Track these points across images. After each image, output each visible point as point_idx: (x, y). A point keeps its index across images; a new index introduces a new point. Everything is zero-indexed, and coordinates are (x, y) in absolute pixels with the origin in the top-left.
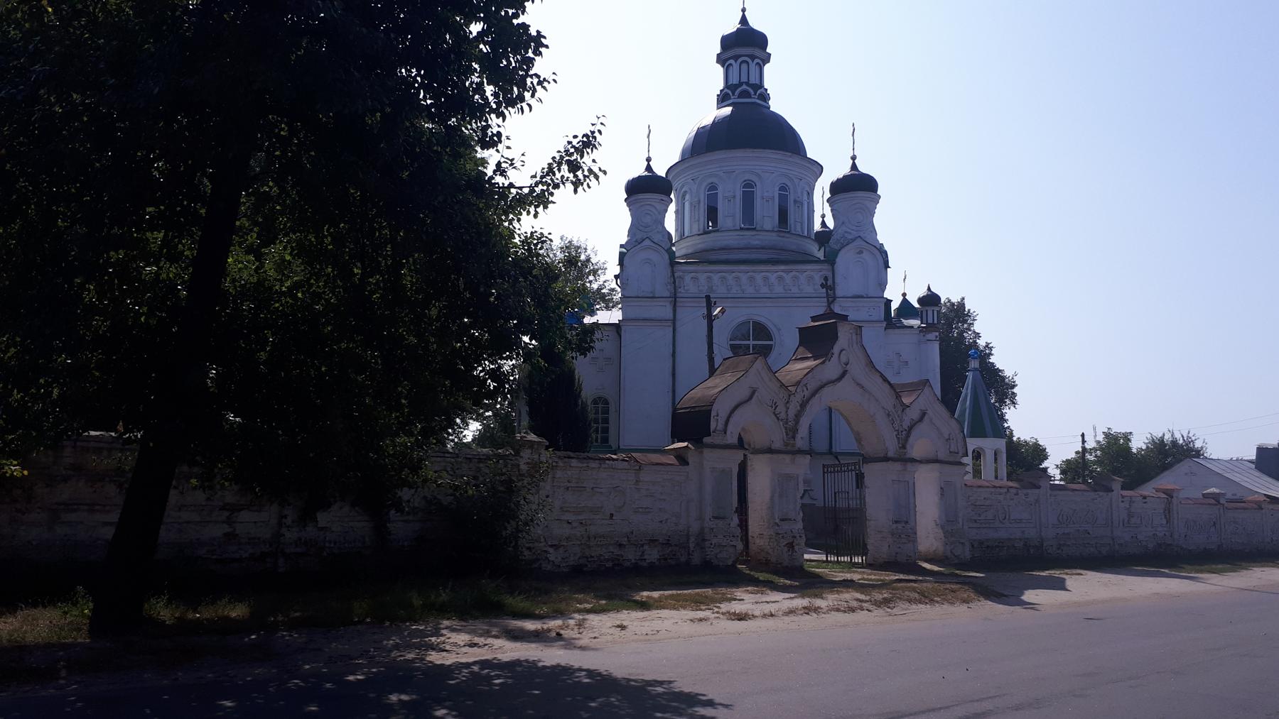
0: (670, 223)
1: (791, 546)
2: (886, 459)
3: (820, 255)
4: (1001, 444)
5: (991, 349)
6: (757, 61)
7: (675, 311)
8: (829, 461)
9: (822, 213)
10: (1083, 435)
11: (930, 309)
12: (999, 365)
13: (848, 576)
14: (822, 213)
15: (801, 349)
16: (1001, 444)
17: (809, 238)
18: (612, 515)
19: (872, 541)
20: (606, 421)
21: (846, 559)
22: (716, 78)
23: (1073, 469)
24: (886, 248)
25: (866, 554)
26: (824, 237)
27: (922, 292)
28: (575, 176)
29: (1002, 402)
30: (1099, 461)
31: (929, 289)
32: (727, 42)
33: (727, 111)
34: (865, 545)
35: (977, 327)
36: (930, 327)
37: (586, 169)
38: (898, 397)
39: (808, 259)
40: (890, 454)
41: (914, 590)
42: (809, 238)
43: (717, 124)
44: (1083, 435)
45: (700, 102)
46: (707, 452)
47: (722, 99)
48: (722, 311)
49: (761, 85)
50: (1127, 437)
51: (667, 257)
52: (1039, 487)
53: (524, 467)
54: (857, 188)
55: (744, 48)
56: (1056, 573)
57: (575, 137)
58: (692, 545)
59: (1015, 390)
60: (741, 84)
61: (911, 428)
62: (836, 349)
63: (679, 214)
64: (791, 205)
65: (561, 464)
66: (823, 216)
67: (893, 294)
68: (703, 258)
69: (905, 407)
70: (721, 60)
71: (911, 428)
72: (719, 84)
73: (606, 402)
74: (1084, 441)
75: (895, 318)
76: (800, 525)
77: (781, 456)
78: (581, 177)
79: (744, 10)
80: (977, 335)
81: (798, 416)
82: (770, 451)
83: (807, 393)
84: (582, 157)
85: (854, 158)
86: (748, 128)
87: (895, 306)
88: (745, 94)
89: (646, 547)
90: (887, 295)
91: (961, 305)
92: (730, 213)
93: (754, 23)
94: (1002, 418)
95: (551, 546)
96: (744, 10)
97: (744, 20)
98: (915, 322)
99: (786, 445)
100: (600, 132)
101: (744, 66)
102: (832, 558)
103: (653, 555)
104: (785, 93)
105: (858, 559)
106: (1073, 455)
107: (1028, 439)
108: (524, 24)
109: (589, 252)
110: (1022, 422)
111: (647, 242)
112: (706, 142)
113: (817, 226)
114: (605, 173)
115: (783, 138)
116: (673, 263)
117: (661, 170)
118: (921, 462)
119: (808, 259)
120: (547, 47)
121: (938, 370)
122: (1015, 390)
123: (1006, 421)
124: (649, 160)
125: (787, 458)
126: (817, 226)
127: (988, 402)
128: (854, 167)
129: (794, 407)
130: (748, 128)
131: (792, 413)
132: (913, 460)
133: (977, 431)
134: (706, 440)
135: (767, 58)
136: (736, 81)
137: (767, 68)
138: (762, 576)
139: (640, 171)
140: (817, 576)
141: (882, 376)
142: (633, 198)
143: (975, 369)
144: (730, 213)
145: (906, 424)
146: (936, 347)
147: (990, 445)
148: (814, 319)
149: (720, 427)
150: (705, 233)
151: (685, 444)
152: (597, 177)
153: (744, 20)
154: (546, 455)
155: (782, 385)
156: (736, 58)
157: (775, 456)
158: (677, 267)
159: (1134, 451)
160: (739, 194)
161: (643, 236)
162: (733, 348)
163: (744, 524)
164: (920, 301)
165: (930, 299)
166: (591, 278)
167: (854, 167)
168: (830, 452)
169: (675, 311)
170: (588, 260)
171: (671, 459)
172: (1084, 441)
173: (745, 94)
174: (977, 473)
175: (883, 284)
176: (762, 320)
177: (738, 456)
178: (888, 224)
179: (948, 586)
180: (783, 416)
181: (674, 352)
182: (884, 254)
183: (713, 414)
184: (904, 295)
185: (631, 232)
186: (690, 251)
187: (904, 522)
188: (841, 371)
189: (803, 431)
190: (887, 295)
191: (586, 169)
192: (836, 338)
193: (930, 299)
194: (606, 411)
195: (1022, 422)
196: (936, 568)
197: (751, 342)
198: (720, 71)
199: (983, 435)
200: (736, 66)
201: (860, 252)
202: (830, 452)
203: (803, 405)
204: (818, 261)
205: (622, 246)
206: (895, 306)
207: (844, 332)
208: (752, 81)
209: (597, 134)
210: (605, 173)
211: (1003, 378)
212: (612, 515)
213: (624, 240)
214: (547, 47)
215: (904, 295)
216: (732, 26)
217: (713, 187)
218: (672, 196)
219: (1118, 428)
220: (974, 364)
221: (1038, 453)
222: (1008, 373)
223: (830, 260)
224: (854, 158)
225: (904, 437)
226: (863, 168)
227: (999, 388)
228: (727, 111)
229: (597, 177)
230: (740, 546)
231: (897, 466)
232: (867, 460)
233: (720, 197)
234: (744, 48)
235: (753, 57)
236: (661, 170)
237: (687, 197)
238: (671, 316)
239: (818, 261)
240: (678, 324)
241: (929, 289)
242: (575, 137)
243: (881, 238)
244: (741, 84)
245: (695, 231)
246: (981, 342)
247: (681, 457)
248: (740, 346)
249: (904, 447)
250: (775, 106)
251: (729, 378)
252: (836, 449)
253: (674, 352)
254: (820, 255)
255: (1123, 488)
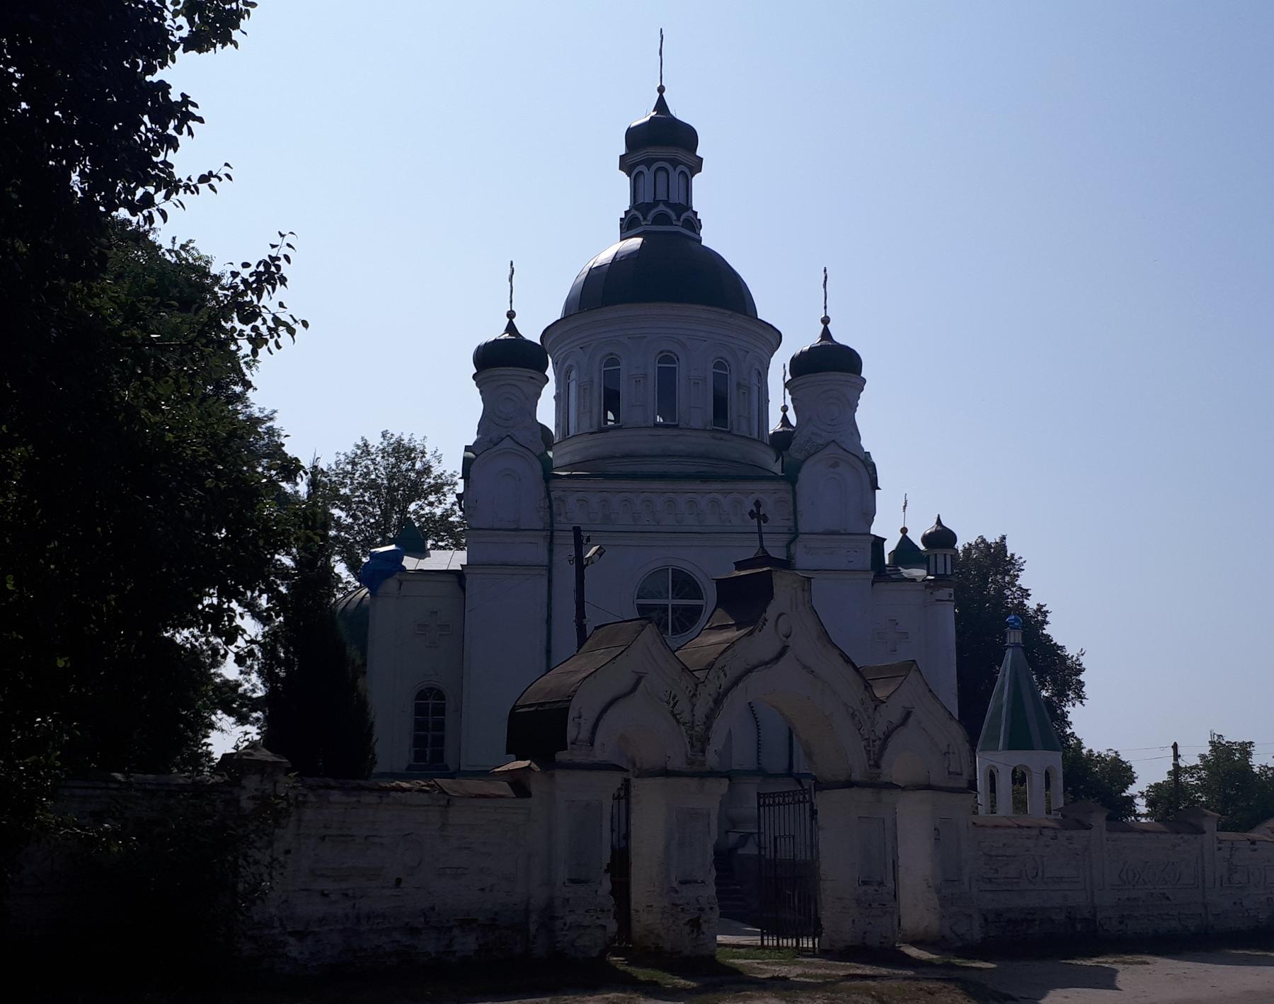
0: (546, 412)
1: (695, 924)
2: (849, 784)
3: (777, 468)
4: (1055, 760)
5: (1045, 614)
6: (681, 168)
7: (551, 551)
8: (788, 785)
9: (779, 405)
10: (1175, 747)
11: (940, 552)
12: (1058, 639)
13: (783, 971)
14: (779, 405)
15: (720, 612)
16: (1055, 760)
17: (760, 441)
18: (399, 881)
19: (827, 916)
20: (440, 726)
21: (791, 942)
22: (617, 193)
23: (1169, 797)
24: (874, 458)
25: (819, 935)
26: (783, 440)
27: (929, 526)
28: (255, 329)
29: (1061, 694)
30: (1203, 788)
31: (939, 522)
32: (635, 137)
33: (635, 243)
34: (818, 920)
35: (1023, 581)
36: (941, 580)
37: (269, 318)
38: (868, 687)
39: (757, 474)
40: (856, 776)
41: (867, 992)
42: (760, 441)
43: (619, 262)
44: (1175, 747)
45: (592, 227)
46: (559, 774)
47: (628, 226)
48: (600, 553)
49: (688, 206)
50: (1246, 749)
51: (538, 466)
52: (1089, 828)
53: (247, 804)
54: (831, 367)
55: (662, 150)
56: (1106, 962)
57: (246, 265)
58: (533, 928)
59: (1082, 677)
60: (656, 203)
61: (888, 736)
62: (772, 611)
63: (561, 399)
64: (734, 392)
65: (312, 798)
66: (785, 409)
67: (887, 527)
68: (597, 470)
69: (878, 703)
70: (626, 164)
71: (888, 736)
72: (622, 202)
73: (440, 695)
74: (1176, 756)
75: (881, 568)
76: (712, 890)
77: (685, 780)
78: (263, 329)
79: (661, 90)
80: (1025, 593)
81: (710, 717)
82: (666, 773)
83: (725, 682)
84: (259, 299)
85: (826, 321)
86: (666, 272)
87: (889, 547)
88: (662, 219)
89: (456, 932)
90: (876, 530)
91: (1001, 546)
92: (638, 395)
93: (678, 110)
94: (1063, 720)
95: (291, 934)
96: (661, 90)
97: (661, 105)
98: (919, 573)
99: (691, 763)
100: (287, 258)
101: (662, 175)
102: (770, 941)
103: (468, 943)
104: (726, 216)
105: (807, 943)
106: (1166, 778)
107: (1104, 753)
108: (161, 82)
109: (428, 457)
110: (1093, 725)
111: (507, 443)
112: (600, 291)
113: (774, 425)
114: (305, 324)
115: (722, 289)
116: (548, 475)
117: (531, 331)
118: (904, 789)
119: (757, 474)
120: (201, 120)
121: (954, 647)
122: (1082, 677)
123: (1069, 724)
124: (511, 315)
125: (693, 783)
126: (774, 425)
127: (1036, 695)
128: (826, 334)
129: (703, 704)
130: (666, 272)
131: (700, 712)
132: (891, 786)
133: (1018, 741)
134: (561, 756)
135: (697, 165)
136: (649, 200)
137: (697, 180)
138: (643, 974)
139: (496, 331)
140: (735, 972)
141: (842, 654)
142: (487, 373)
143: (1017, 645)
144: (638, 395)
145: (880, 730)
146: (949, 613)
147: (1040, 761)
148: (740, 565)
149: (584, 735)
150: (603, 430)
151: (526, 763)
152: (292, 332)
153: (661, 105)
154: (286, 784)
155: (685, 668)
156: (648, 163)
157: (671, 780)
158: (555, 484)
159: (1256, 770)
160: (652, 372)
161: (503, 428)
162: (641, 608)
163: (621, 890)
164: (926, 539)
165: (941, 537)
166: (432, 498)
167: (826, 334)
168: (789, 773)
169: (551, 551)
170: (427, 470)
171: (503, 788)
172: (1176, 756)
173: (662, 219)
174: (1020, 803)
175: (869, 513)
176: (686, 567)
177: (616, 779)
178: (877, 422)
179: (924, 984)
180: (686, 717)
181: (549, 617)
182: (870, 468)
183: (572, 714)
184: (904, 530)
185: (484, 426)
186: (577, 459)
187: (879, 887)
188: (777, 647)
189: (717, 742)
190: (876, 530)
191: (269, 318)
192: (770, 595)
193: (941, 537)
194: (441, 710)
195: (1093, 725)
196: (925, 955)
197: (671, 602)
198: (624, 181)
199: (1028, 746)
200: (649, 174)
201: (835, 465)
202: (789, 773)
203: (718, 701)
204: (774, 478)
205: (467, 448)
206: (889, 547)
207: (783, 585)
208: (674, 199)
209: (283, 263)
210: (305, 324)
211: (1065, 658)
212: (399, 881)
213: (471, 438)
214: (201, 120)
215: (904, 530)
216: (643, 114)
217: (613, 361)
218: (550, 372)
219: (1233, 736)
220: (1014, 637)
221: (1120, 772)
222: (1071, 651)
223: (790, 476)
224: (826, 321)
225: (877, 751)
226: (840, 337)
227: (1062, 674)
228: (635, 243)
229: (292, 332)
230: (613, 927)
231: (867, 794)
232: (822, 785)
233: (623, 377)
234: (662, 150)
235: (675, 163)
236: (531, 331)
237: (573, 374)
238: (546, 562)
239: (774, 478)
240: (555, 571)
241: (939, 522)
242: (246, 265)
243: (867, 444)
244: (656, 203)
245: (586, 427)
246: (1031, 604)
247: (519, 784)
248: (652, 608)
249: (877, 766)
250: (709, 238)
251: (601, 656)
252: (801, 766)
253: (549, 617)
254: (777, 468)
255: (1223, 828)
